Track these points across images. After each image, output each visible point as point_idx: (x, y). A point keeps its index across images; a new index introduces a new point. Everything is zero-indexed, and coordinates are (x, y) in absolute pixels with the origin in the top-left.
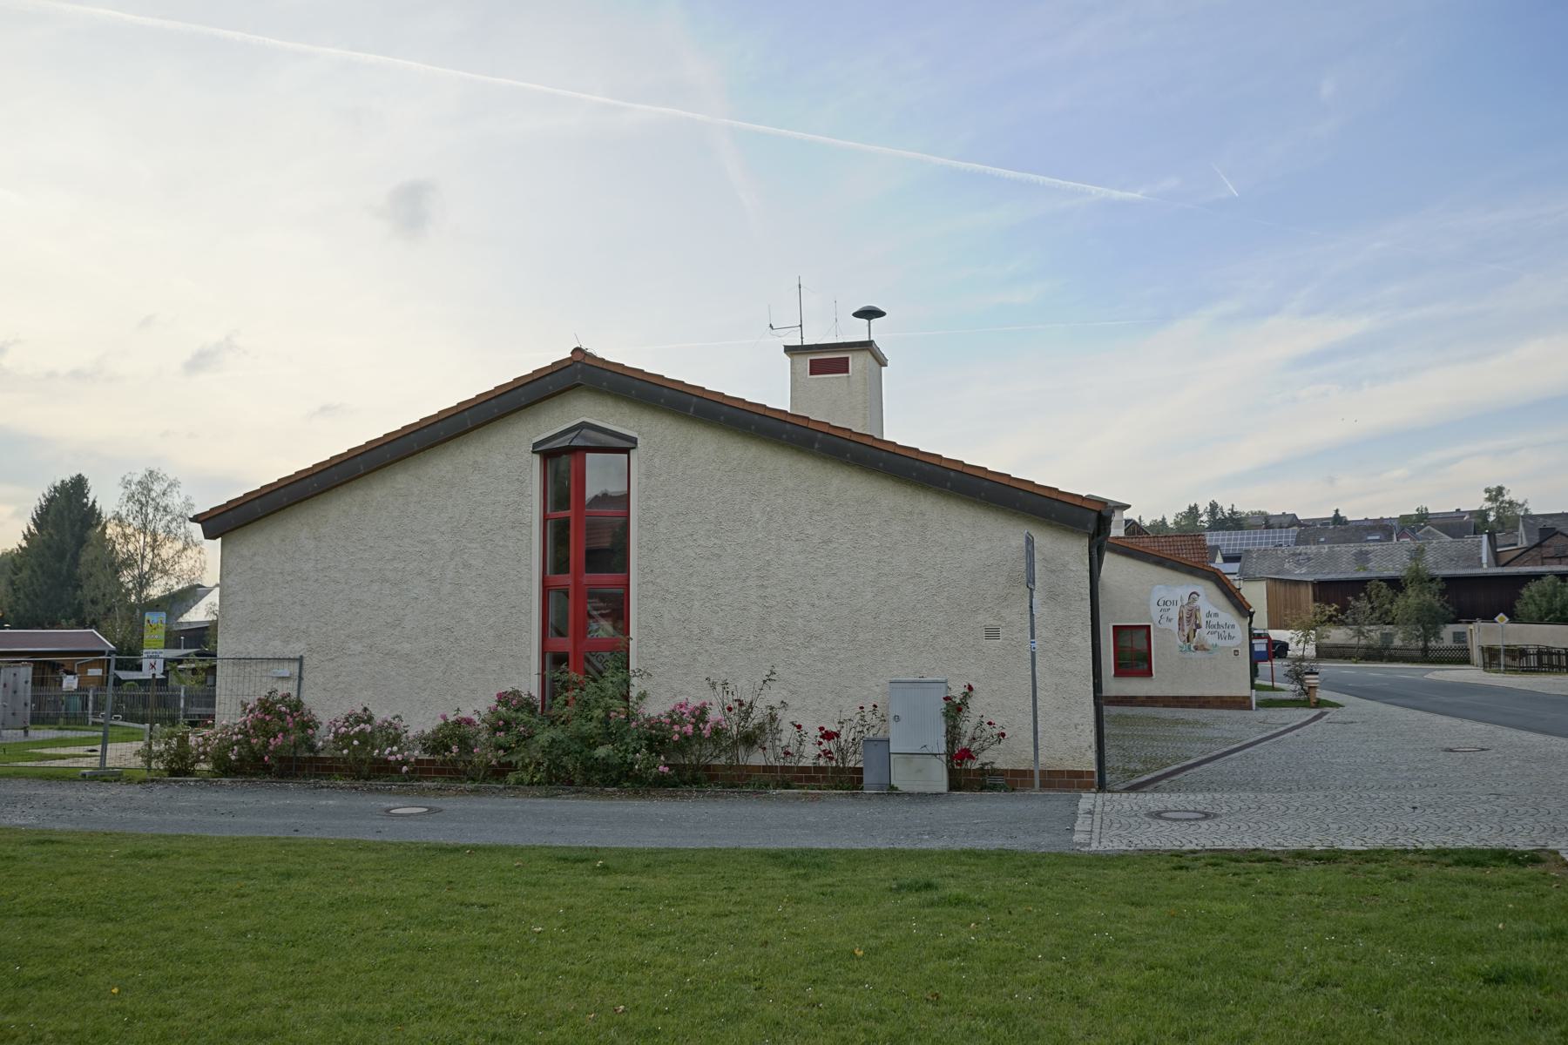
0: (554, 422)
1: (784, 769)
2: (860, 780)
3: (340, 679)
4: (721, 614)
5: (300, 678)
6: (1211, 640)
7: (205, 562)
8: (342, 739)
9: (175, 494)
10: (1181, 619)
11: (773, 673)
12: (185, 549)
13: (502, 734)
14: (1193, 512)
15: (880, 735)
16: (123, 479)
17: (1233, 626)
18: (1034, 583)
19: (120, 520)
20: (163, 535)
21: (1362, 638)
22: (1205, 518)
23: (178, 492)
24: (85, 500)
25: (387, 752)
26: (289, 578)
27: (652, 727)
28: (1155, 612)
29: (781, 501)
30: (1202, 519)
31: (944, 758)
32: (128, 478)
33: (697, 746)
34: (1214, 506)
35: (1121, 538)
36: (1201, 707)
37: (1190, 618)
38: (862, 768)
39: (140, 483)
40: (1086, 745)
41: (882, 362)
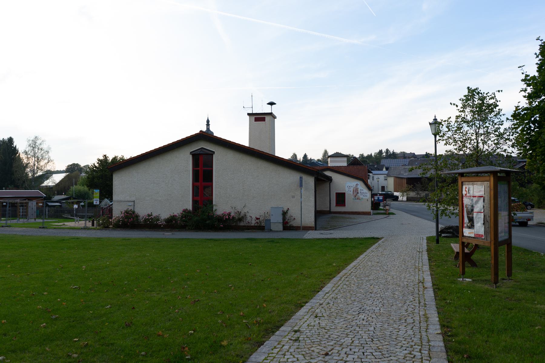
0: (195, 147)
1: (248, 226)
2: (264, 228)
3: (144, 206)
4: (234, 192)
5: (134, 206)
6: (361, 197)
7: (55, 167)
8: (146, 220)
9: (44, 144)
10: (353, 191)
11: (245, 205)
12: (48, 162)
13: (184, 218)
14: (381, 152)
15: (269, 219)
16: (27, 139)
17: (367, 193)
18: (302, 186)
19: (26, 153)
20: (41, 158)
21: (418, 195)
22: (384, 154)
23: (45, 144)
24: (13, 145)
25: (158, 222)
26: (131, 182)
27: (219, 217)
28: (347, 189)
29: (247, 167)
30: (383, 154)
31: (282, 223)
32: (29, 139)
33: (229, 221)
34: (387, 150)
35: (346, 166)
36: (358, 214)
37: (356, 191)
38: (264, 226)
39: (33, 140)
40: (312, 221)
41: (275, 117)
